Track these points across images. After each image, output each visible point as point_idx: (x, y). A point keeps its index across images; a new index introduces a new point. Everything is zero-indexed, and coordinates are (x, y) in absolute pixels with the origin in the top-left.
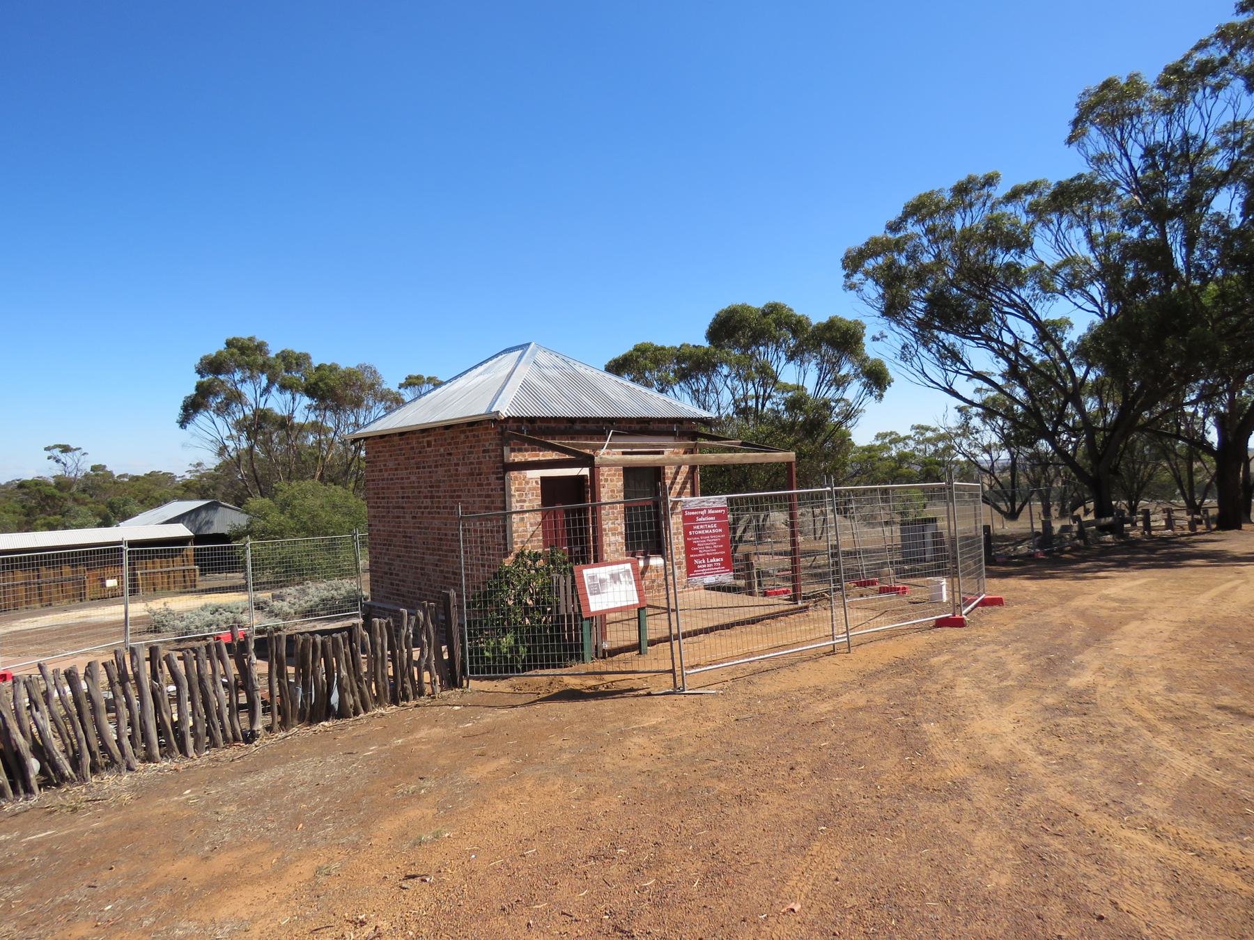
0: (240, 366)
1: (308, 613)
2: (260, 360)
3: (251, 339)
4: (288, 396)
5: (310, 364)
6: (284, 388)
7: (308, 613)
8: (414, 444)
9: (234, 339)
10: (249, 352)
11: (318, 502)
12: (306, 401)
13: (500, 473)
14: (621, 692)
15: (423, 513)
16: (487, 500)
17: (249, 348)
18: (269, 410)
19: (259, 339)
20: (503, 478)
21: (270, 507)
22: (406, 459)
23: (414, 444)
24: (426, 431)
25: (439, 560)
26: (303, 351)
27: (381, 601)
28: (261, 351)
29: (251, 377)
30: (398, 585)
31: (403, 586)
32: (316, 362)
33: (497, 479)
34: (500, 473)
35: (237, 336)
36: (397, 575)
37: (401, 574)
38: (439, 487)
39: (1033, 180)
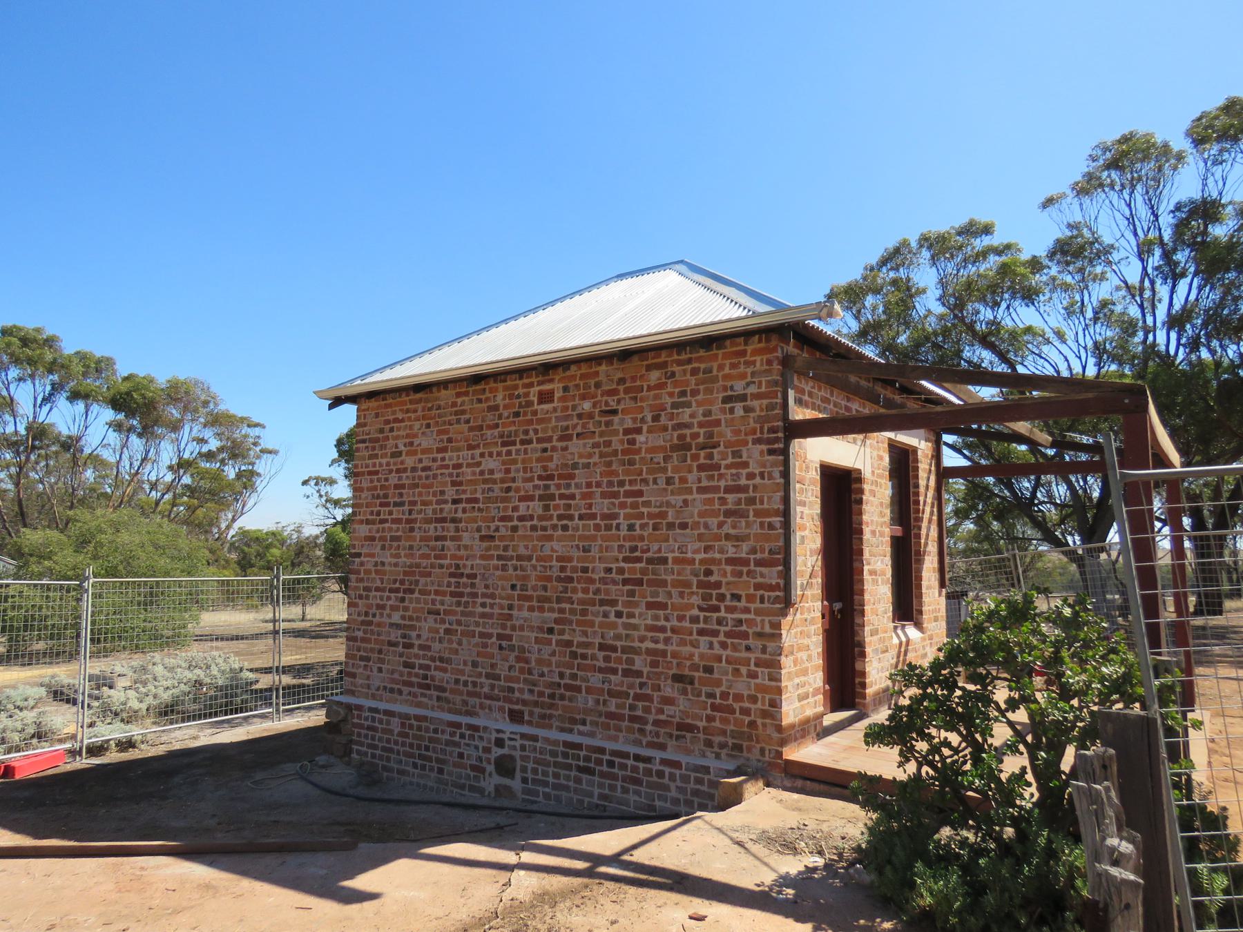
0: (17, 361)
1: (169, 712)
2: (49, 357)
3: (38, 330)
4: (80, 406)
5: (114, 373)
6: (74, 396)
7: (169, 712)
8: (500, 399)
9: (15, 326)
10: (34, 346)
11: (137, 539)
12: (109, 414)
13: (777, 440)
14: (746, 848)
15: (515, 529)
16: (731, 498)
17: (35, 341)
18: (52, 425)
19: (49, 332)
20: (785, 452)
21: (59, 543)
22: (471, 429)
23: (500, 399)
24: (548, 368)
25: (557, 621)
26: (107, 354)
27: (374, 697)
28: (51, 347)
29: (32, 376)
30: (428, 668)
31: (445, 670)
32: (123, 370)
33: (771, 452)
34: (777, 440)
35: (19, 324)
36: (427, 648)
37: (436, 646)
38: (572, 477)
39: (1005, 242)
